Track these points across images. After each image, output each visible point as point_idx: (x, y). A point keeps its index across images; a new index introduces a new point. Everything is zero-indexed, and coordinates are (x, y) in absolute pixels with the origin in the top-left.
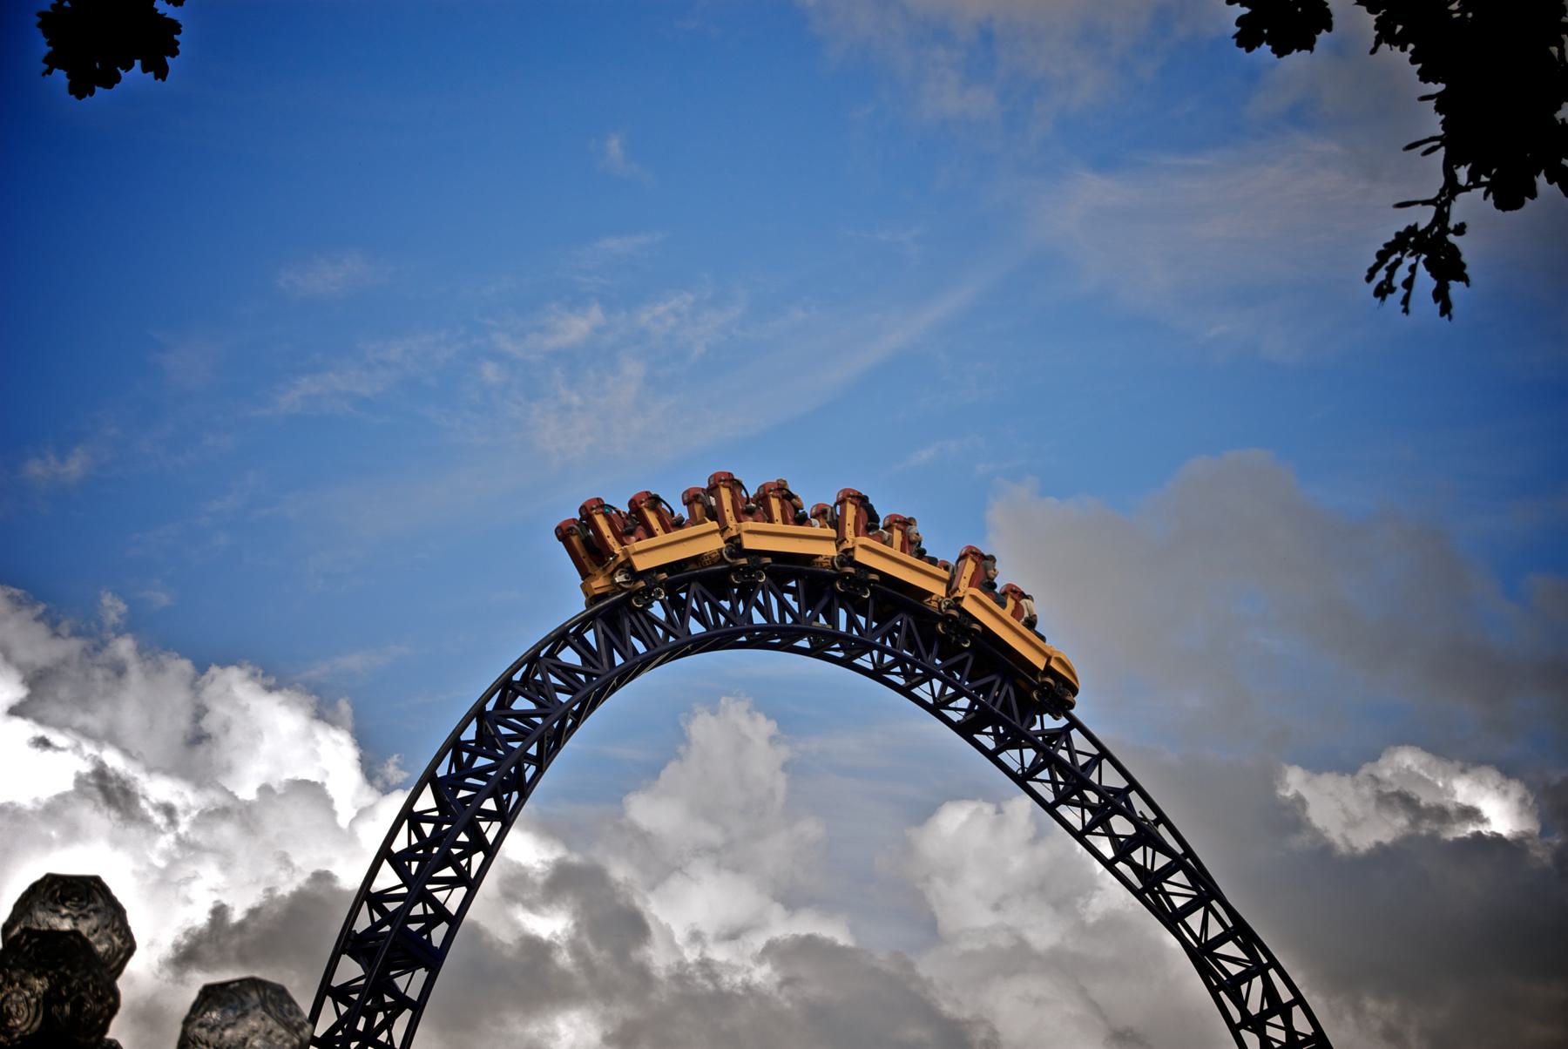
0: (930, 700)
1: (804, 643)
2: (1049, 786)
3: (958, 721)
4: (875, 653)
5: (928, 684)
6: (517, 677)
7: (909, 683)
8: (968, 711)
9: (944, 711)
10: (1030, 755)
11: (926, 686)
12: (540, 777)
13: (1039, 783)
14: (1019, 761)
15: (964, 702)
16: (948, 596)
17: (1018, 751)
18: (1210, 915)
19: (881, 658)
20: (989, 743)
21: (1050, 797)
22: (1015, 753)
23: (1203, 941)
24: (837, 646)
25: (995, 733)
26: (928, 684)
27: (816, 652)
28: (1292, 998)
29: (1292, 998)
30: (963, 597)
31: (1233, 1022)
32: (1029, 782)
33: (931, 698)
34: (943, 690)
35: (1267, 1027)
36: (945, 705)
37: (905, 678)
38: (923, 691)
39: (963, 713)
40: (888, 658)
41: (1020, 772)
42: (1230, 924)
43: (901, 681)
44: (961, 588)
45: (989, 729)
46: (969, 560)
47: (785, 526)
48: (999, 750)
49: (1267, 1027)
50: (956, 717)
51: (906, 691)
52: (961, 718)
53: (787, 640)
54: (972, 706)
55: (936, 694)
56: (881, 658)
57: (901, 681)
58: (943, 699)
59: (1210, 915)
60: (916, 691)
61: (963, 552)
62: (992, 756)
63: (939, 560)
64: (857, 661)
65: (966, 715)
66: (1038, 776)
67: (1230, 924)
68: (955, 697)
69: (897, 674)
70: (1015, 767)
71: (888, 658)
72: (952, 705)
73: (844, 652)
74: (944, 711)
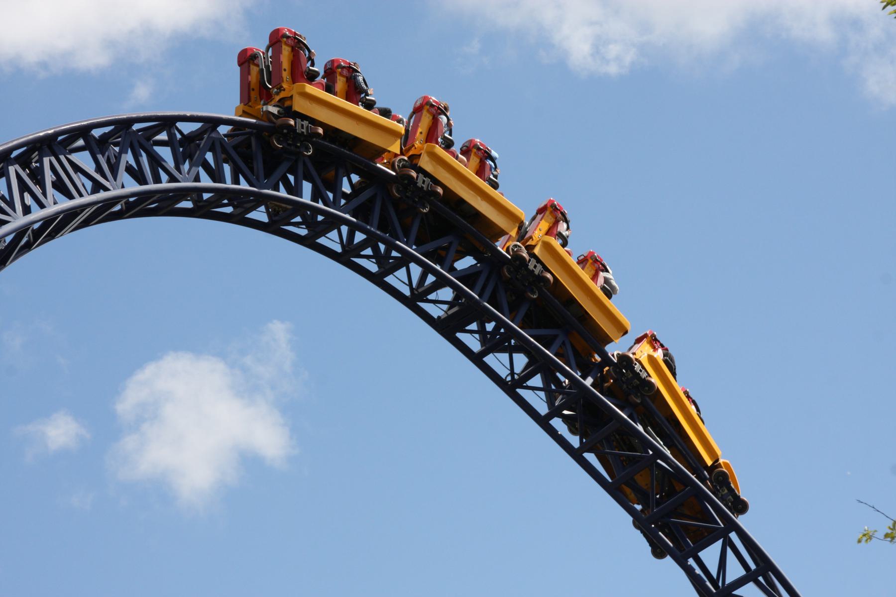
0: (406, 291)
1: (260, 215)
2: (542, 394)
3: (439, 317)
4: (344, 229)
5: (404, 269)
6: (97, 133)
7: (382, 270)
8: (451, 304)
9: (423, 305)
10: (521, 361)
11: (402, 273)
12: (50, 240)
13: (531, 391)
14: (508, 365)
15: (446, 294)
16: (402, 153)
17: (507, 355)
18: (729, 551)
19: (351, 235)
20: (474, 343)
21: (543, 409)
22: (504, 357)
23: (720, 584)
24: (298, 219)
25: (482, 331)
26: (404, 269)
27: (273, 227)
28: (429, 275)
29: (429, 275)
30: (420, 155)
31: (434, 318)
32: (518, 390)
33: (408, 288)
34: (423, 278)
35: (404, 269)
36: (423, 297)
37: (378, 263)
38: (398, 279)
39: (445, 307)
40: (359, 237)
41: (509, 379)
42: (753, 566)
43: (373, 267)
44: (417, 144)
45: (474, 326)
46: (425, 112)
47: (577, 265)
48: (484, 353)
49: (404, 269)
50: (435, 311)
51: (378, 279)
52: (441, 313)
53: (239, 211)
54: (456, 298)
55: (414, 285)
56: (351, 235)
57: (373, 267)
58: (420, 290)
59: (729, 551)
60: (390, 279)
61: (418, 104)
62: (477, 359)
63: (393, 114)
64: (322, 241)
65: (449, 309)
66: (530, 383)
67: (753, 566)
68: (435, 287)
69: (367, 257)
70: (503, 373)
71: (359, 237)
72: (432, 297)
73: (307, 228)
74: (423, 305)
